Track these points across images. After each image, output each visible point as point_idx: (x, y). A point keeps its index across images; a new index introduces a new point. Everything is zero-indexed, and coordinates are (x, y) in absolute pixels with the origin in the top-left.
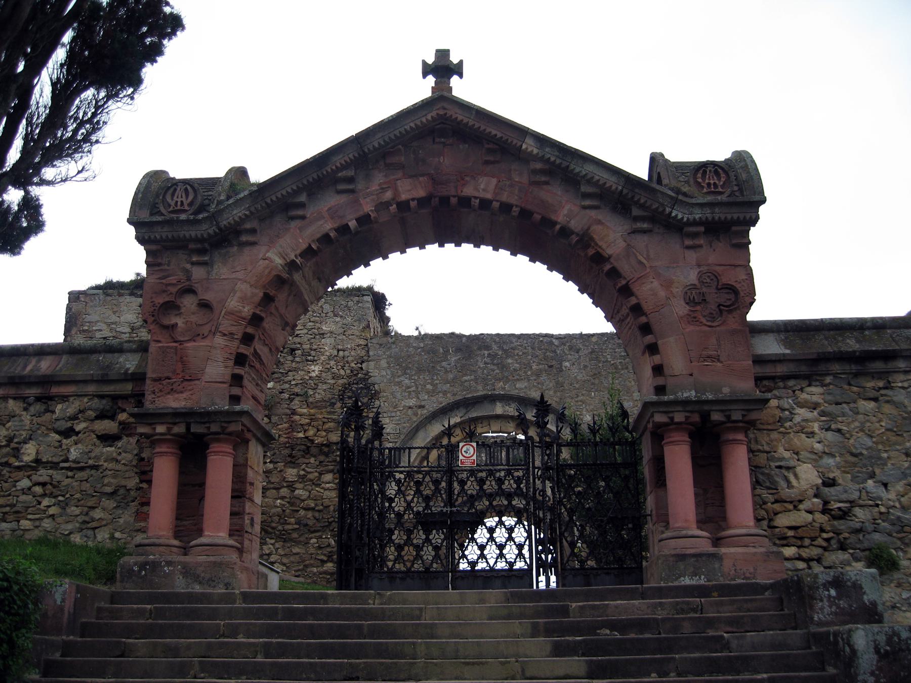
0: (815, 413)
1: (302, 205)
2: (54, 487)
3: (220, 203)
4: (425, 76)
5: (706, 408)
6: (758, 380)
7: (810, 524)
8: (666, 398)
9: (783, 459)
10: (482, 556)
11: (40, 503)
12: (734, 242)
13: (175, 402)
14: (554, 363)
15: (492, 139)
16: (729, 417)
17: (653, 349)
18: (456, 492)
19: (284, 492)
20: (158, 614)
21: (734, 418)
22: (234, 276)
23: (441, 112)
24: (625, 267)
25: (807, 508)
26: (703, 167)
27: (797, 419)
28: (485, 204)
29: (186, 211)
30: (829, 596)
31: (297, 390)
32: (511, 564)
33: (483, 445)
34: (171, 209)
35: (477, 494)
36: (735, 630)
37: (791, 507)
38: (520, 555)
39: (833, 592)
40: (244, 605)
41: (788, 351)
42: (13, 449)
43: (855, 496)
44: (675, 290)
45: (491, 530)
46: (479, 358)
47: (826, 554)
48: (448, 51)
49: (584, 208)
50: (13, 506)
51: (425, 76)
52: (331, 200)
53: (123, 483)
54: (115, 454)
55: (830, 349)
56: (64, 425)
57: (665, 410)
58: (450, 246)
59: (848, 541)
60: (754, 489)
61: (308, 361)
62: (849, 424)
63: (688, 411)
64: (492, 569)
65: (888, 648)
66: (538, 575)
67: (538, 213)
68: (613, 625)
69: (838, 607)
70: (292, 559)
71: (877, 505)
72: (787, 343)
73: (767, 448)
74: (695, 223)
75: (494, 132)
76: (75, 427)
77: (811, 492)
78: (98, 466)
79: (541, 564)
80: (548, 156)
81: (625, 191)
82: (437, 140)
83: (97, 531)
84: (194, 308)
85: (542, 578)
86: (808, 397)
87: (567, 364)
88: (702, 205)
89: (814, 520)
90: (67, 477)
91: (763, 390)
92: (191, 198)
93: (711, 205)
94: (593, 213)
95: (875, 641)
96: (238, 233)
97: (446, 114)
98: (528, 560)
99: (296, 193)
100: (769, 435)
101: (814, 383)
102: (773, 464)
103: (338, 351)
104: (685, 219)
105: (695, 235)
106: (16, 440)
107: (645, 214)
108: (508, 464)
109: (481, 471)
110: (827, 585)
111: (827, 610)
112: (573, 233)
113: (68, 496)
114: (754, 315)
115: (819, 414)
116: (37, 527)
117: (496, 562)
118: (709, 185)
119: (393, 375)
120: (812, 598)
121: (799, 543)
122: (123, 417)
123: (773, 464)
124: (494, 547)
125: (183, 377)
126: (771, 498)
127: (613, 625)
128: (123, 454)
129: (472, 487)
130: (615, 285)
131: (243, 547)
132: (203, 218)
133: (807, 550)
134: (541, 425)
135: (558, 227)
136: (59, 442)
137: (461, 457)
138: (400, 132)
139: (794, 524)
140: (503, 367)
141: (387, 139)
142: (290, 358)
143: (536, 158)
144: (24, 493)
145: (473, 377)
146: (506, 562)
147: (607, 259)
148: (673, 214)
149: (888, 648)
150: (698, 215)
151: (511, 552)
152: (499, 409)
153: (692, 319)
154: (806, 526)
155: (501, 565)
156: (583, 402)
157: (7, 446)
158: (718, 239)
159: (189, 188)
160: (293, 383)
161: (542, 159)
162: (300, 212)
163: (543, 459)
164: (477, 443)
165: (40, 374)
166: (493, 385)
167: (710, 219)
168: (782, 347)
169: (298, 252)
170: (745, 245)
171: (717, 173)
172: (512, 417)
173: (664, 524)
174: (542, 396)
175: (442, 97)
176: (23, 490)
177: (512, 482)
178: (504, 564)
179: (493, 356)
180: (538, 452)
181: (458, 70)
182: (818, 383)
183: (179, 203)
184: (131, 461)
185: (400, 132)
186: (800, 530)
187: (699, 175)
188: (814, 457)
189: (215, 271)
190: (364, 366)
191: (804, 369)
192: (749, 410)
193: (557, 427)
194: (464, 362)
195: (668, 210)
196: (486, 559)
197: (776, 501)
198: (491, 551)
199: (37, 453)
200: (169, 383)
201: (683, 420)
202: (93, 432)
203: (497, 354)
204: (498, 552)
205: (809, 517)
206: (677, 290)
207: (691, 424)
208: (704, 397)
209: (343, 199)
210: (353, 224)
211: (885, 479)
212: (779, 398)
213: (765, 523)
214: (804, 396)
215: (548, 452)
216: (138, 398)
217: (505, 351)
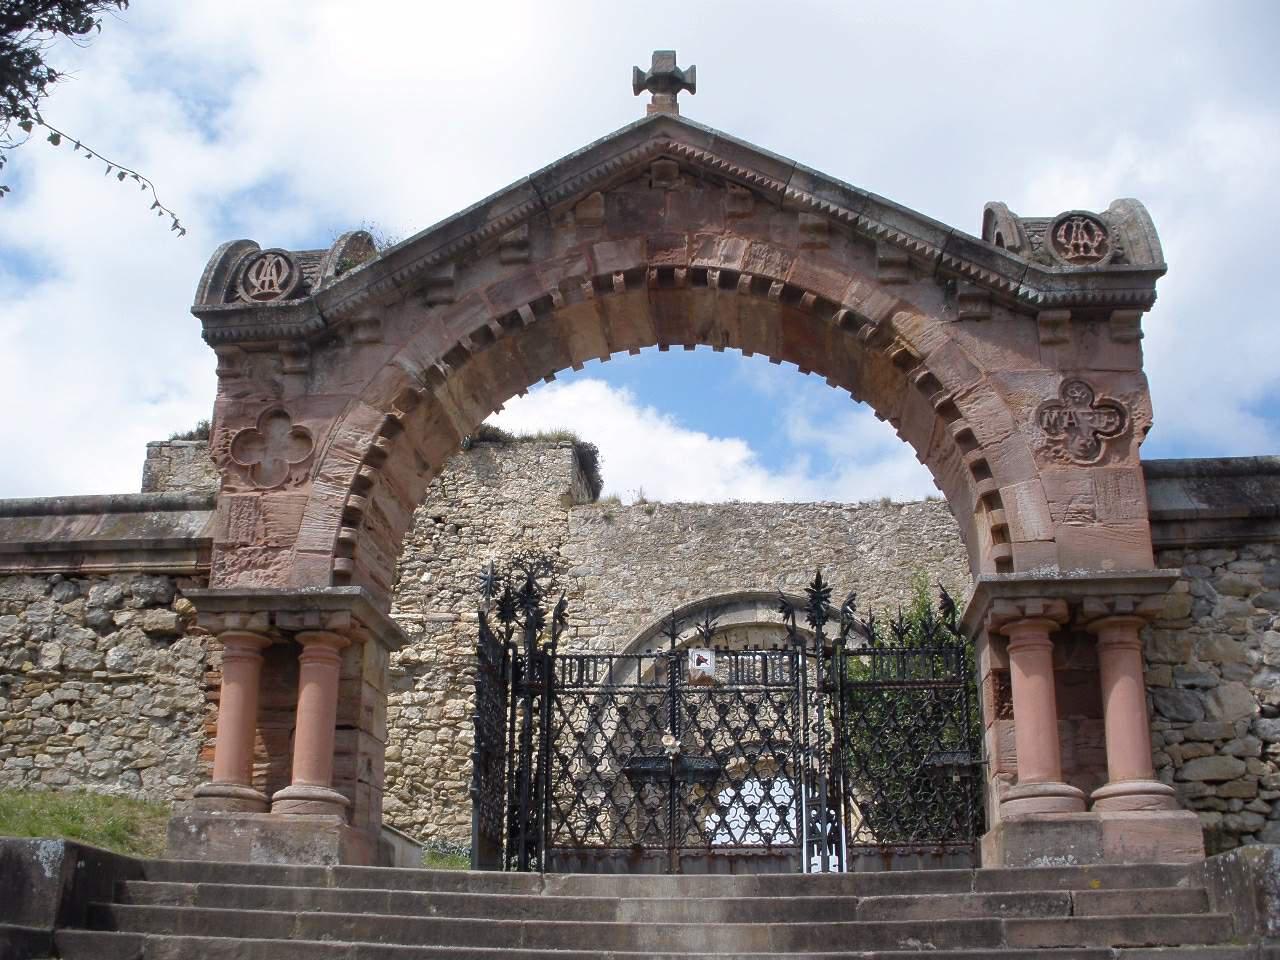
0: (1249, 602)
1: (448, 284)
2: (85, 706)
3: (325, 281)
4: (638, 90)
5: (1076, 591)
6: (1158, 551)
7: (1243, 776)
9: (1198, 674)
11: (64, 730)
12: (1117, 335)
13: (249, 581)
15: (739, 181)
16: (1111, 606)
19: (443, 733)
20: (203, 896)
21: (1120, 608)
22: (344, 391)
23: (662, 141)
24: (945, 373)
28: (729, 279)
29: (276, 295)
31: (464, 584)
32: (768, 838)
34: (256, 292)
36: (1129, 943)
37: (1210, 749)
38: (783, 823)
40: (338, 889)
42: (30, 649)
46: (732, 540)
47: (1270, 824)
50: (26, 733)
51: (638, 90)
52: (491, 274)
53: (181, 704)
54: (170, 660)
56: (98, 615)
58: (677, 349)
60: (1151, 720)
61: (479, 542)
66: (810, 854)
70: (455, 830)
73: (1171, 657)
74: (1057, 305)
76: (115, 619)
77: (1241, 727)
78: (146, 676)
80: (824, 204)
81: (946, 257)
83: (143, 773)
84: (286, 440)
85: (817, 859)
86: (1236, 577)
87: (863, 547)
88: (1066, 277)
89: (1247, 771)
90: (104, 692)
92: (284, 275)
93: (1082, 277)
96: (352, 327)
98: (794, 832)
99: (441, 264)
101: (1244, 556)
102: (1181, 683)
103: (524, 528)
104: (1040, 299)
105: (1055, 325)
106: (34, 637)
108: (765, 683)
112: (865, 320)
113: (103, 720)
115: (1254, 603)
116: (59, 765)
117: (744, 835)
118: (1076, 247)
119: (606, 565)
121: (1224, 806)
122: (182, 603)
123: (1181, 683)
124: (742, 811)
125: (266, 543)
126: (1179, 736)
128: (183, 660)
131: (354, 804)
132: (300, 305)
133: (1238, 819)
135: (843, 312)
136: (93, 640)
138: (598, 172)
140: (767, 551)
141: (578, 182)
142: (454, 538)
143: (809, 208)
144: (42, 715)
146: (761, 834)
147: (920, 361)
148: (1021, 292)
150: (1060, 291)
151: (768, 819)
154: (1236, 779)
155: (752, 839)
157: (21, 645)
159: (281, 259)
160: (457, 575)
162: (445, 294)
163: (820, 672)
165: (70, 539)
167: (1079, 298)
168: (1195, 500)
169: (442, 354)
170: (1132, 339)
171: (1087, 228)
176: (40, 709)
178: (756, 837)
179: (753, 537)
182: (1251, 556)
183: (267, 284)
184: (194, 670)
185: (598, 172)
186: (1225, 786)
187: (1062, 232)
189: (317, 383)
190: (562, 550)
192: (1143, 596)
195: (1013, 286)
196: (729, 829)
197: (1187, 740)
199: (62, 658)
200: (245, 553)
201: (1041, 611)
202: (140, 626)
204: (747, 818)
205: (1241, 766)
207: (1052, 618)
208: (1072, 575)
209: (509, 272)
210: (525, 311)
214: (1227, 577)
216: (204, 577)
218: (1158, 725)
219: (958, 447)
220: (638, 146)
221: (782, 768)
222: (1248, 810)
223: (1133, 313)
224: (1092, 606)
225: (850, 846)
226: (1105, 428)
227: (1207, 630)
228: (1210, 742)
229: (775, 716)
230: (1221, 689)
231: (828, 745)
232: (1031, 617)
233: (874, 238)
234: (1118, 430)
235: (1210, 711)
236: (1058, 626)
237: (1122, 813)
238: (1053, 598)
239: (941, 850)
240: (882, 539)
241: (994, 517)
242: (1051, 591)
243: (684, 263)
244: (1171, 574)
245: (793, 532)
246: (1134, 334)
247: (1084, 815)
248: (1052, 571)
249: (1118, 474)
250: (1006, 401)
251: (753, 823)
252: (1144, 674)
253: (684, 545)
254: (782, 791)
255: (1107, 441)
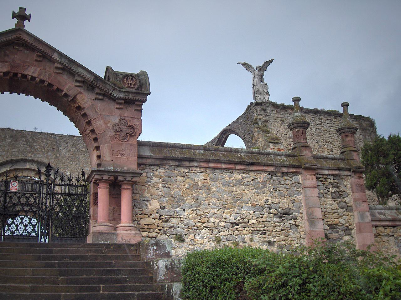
0: (161, 180)
6: (139, 165)
8: (101, 169)
9: (145, 197)
10: (17, 230)
14: (55, 147)
15: (39, 51)
17: (98, 148)
18: (7, 202)
24: (89, 112)
25: (153, 217)
26: (127, 76)
27: (153, 182)
30: (153, 248)
32: (30, 234)
33: (21, 182)
35: (17, 203)
37: (147, 216)
38: (34, 230)
39: (155, 248)
41: (152, 155)
43: (172, 214)
44: (109, 125)
45: (22, 219)
46: (21, 141)
47: (159, 235)
48: (25, 9)
49: (76, 86)
55: (169, 155)
57: (100, 174)
58: (15, 94)
59: (168, 231)
60: (133, 208)
62: (173, 185)
63: (109, 175)
64: (21, 235)
65: (170, 267)
67: (55, 86)
68: (71, 258)
69: (156, 253)
71: (180, 218)
72: (153, 151)
73: (140, 193)
75: (41, 48)
77: (155, 211)
79: (42, 234)
82: (15, 47)
87: (61, 148)
91: (141, 169)
94: (79, 89)
95: (166, 264)
97: (20, 37)
98: (37, 232)
100: (141, 187)
101: (161, 168)
102: (142, 199)
104: (117, 97)
107: (101, 92)
109: (19, 193)
110: (153, 245)
111: (152, 254)
112: (69, 96)
114: (141, 138)
117: (23, 233)
118: (128, 84)
120: (147, 249)
121: (149, 230)
123: (142, 199)
127: (71, 258)
129: (15, 200)
130: (85, 120)
133: (152, 234)
134: (48, 176)
135: (64, 93)
137: (11, 187)
139: (148, 223)
140: (31, 147)
143: (58, 62)
145: (17, 150)
149: (170, 267)
150: (122, 95)
152: (28, 166)
153: (113, 138)
156: (67, 166)
158: (130, 106)
161: (60, 63)
163: (47, 190)
164: (19, 181)
166: (26, 154)
168: (151, 153)
171: (132, 79)
172: (34, 170)
173: (95, 220)
174: (49, 163)
175: (19, 29)
177: (33, 198)
178: (26, 233)
179: (27, 142)
180: (45, 187)
181: (28, 18)
182: (163, 168)
187: (125, 79)
188: (158, 197)
191: (158, 162)
193: (54, 177)
194: (13, 142)
195: (110, 92)
196: (19, 231)
197: (142, 214)
198: (21, 228)
201: (107, 179)
203: (29, 141)
206: (110, 125)
207: (110, 180)
211: (184, 208)
212: (147, 173)
213: (136, 222)
214: (157, 173)
215: (49, 187)
217: (34, 140)
218: (135, 209)
219: (90, 133)
220: (11, 36)
221: (35, 215)
222: (154, 232)
223: (141, 103)
224: (120, 178)
225: (52, 237)
226: (129, 132)
227: (150, 186)
228: (147, 215)
229: (34, 201)
230: (151, 201)
231: (48, 209)
232: (104, 180)
233: (75, 73)
234: (134, 132)
235: (148, 207)
236: (111, 183)
237: (123, 231)
238: (111, 175)
239: (302, 274)
240: (68, 146)
241: (98, 153)
242: (110, 174)
243: (21, 72)
244: (141, 172)
245: (40, 141)
246: (140, 108)
247: (114, 231)
248: (112, 168)
249: (131, 145)
250: (104, 122)
251: (25, 230)
252: (132, 196)
253: (5, 142)
254: (34, 221)
255: (129, 136)
